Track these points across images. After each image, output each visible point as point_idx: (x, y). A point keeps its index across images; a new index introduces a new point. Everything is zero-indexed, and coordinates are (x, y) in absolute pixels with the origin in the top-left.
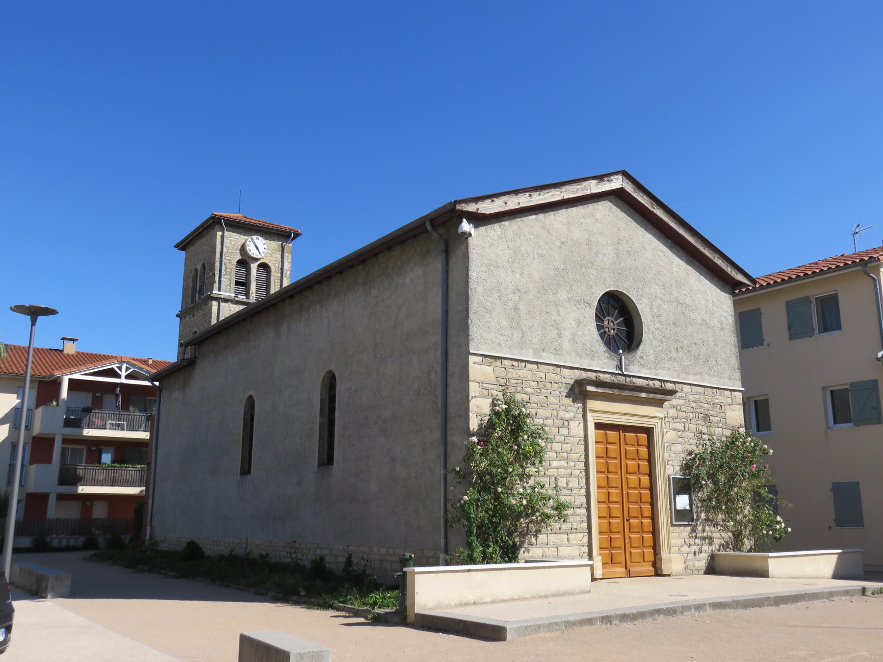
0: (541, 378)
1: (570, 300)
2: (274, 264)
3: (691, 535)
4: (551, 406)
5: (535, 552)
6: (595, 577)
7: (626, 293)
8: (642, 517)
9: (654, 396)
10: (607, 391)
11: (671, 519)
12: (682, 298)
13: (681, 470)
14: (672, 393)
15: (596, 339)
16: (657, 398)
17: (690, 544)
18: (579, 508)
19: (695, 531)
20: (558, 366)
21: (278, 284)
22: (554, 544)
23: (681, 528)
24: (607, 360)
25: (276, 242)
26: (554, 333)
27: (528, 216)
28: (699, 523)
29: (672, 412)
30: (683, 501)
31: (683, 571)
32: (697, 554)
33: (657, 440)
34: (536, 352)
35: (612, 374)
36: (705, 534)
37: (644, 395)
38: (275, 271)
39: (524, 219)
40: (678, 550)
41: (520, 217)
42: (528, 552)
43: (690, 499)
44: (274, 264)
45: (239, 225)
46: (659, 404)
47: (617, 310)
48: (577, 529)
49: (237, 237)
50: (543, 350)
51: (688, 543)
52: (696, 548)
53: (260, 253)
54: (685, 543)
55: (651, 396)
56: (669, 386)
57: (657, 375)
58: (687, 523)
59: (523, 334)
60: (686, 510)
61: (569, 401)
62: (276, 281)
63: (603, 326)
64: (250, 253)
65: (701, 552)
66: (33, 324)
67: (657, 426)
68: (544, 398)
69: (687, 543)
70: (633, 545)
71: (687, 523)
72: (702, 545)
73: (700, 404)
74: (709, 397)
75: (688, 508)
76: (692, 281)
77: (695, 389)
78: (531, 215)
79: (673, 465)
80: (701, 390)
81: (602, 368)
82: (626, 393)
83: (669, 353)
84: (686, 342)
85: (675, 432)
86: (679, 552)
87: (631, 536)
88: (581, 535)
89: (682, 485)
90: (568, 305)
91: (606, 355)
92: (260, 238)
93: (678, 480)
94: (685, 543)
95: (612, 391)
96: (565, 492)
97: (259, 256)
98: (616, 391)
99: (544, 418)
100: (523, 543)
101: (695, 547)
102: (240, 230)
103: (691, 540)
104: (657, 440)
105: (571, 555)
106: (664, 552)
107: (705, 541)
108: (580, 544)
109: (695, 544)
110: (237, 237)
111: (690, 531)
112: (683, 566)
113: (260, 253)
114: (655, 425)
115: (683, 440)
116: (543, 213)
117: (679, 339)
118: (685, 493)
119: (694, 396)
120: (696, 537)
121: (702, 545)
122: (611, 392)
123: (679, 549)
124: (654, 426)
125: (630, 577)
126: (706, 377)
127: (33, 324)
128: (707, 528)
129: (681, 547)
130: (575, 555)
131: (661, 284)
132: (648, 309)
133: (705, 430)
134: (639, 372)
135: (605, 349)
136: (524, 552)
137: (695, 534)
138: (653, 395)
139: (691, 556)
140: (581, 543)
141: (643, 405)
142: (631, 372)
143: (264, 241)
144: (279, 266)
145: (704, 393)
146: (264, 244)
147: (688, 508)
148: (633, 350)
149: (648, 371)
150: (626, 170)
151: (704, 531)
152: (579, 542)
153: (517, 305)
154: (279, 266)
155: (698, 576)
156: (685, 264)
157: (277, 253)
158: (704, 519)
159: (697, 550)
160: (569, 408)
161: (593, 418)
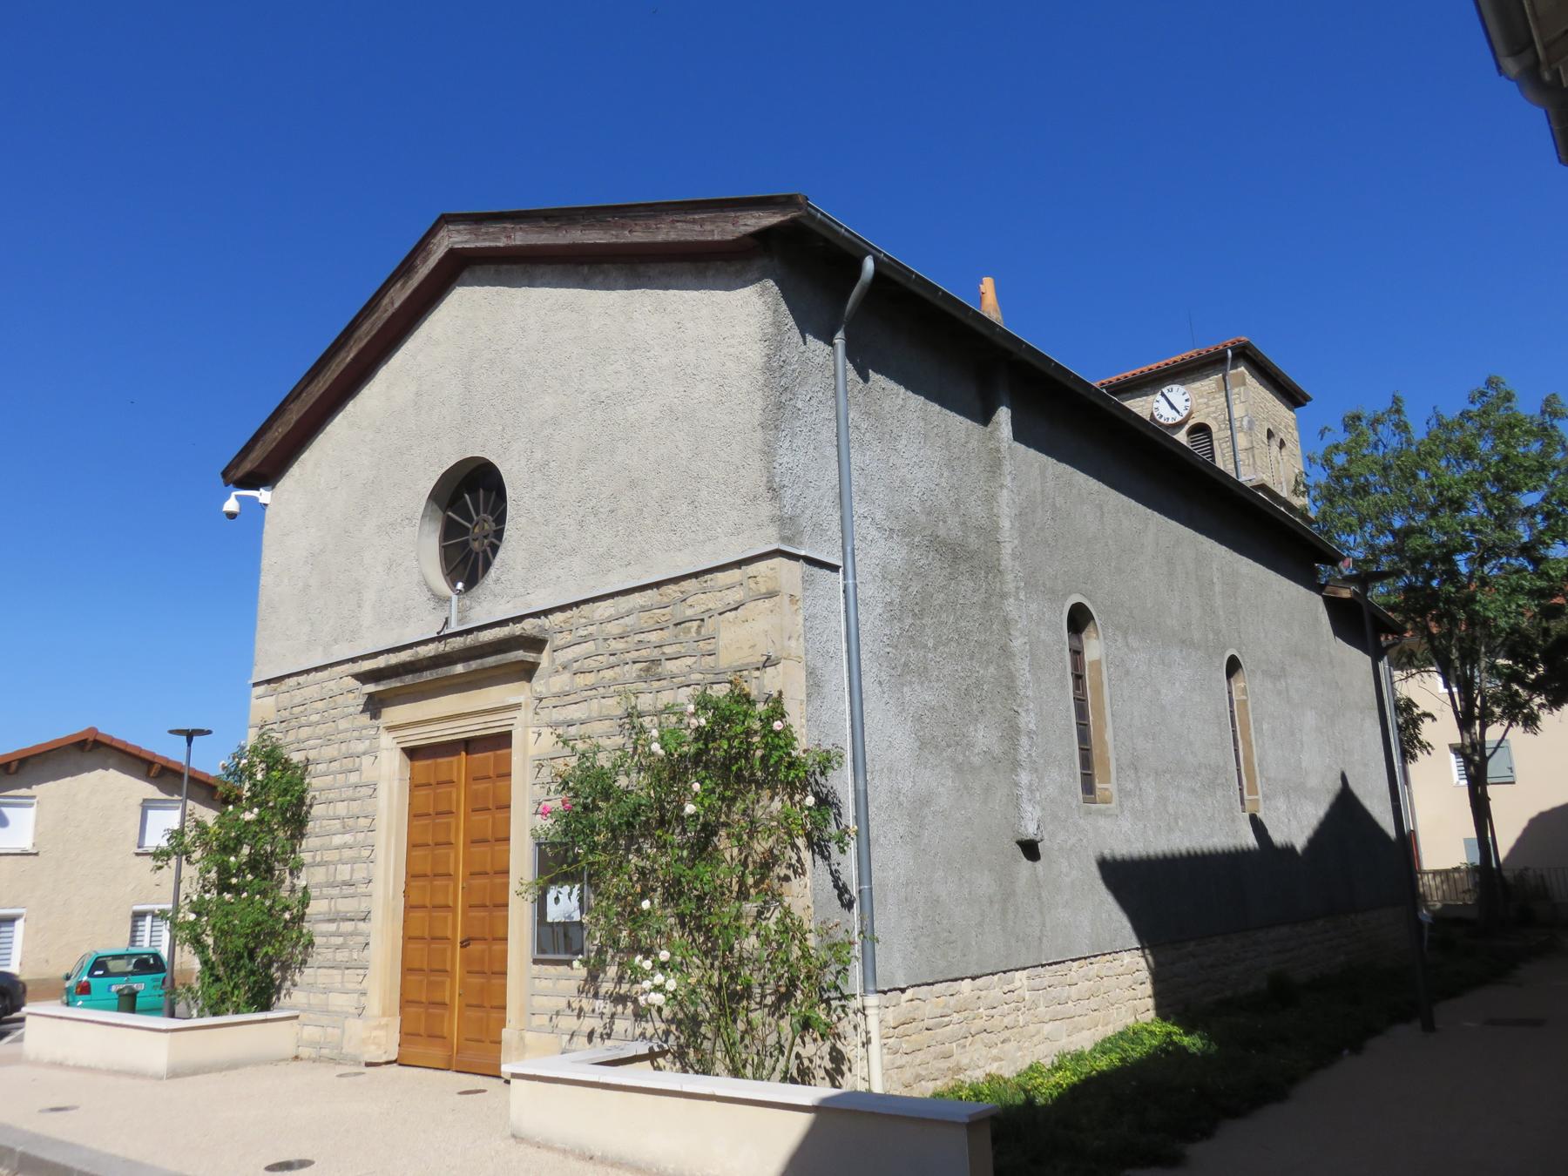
0: (332, 690)
2: (1215, 418)
5: (298, 997)
9: (482, 664)
10: (393, 685)
16: (487, 666)
17: (581, 1009)
21: (1229, 450)
25: (1211, 378)
29: (561, 682)
30: (564, 904)
32: (597, 1040)
37: (459, 668)
38: (1220, 430)
41: (321, 432)
42: (290, 997)
44: (1215, 418)
45: (1188, 366)
46: (527, 672)
49: (1141, 404)
51: (575, 1005)
52: (597, 1024)
53: (1178, 412)
54: (569, 1005)
55: (474, 665)
56: (529, 627)
62: (1224, 445)
64: (1162, 420)
65: (609, 1036)
66: (189, 745)
69: (574, 1006)
80: (735, 574)
82: (428, 676)
92: (1175, 387)
94: (569, 1005)
95: (401, 682)
97: (1179, 418)
98: (409, 679)
100: (284, 979)
101: (592, 1020)
102: (1146, 389)
107: (625, 1007)
109: (593, 1011)
110: (1141, 404)
113: (1178, 412)
121: (613, 1016)
122: (399, 685)
127: (189, 745)
130: (55, 1007)
136: (285, 996)
138: (479, 661)
141: (480, 688)
143: (1182, 389)
144: (1225, 417)
146: (1184, 394)
148: (483, 576)
150: (444, 212)
154: (1225, 417)
157: (1216, 396)
159: (599, 1030)
161: (396, 741)
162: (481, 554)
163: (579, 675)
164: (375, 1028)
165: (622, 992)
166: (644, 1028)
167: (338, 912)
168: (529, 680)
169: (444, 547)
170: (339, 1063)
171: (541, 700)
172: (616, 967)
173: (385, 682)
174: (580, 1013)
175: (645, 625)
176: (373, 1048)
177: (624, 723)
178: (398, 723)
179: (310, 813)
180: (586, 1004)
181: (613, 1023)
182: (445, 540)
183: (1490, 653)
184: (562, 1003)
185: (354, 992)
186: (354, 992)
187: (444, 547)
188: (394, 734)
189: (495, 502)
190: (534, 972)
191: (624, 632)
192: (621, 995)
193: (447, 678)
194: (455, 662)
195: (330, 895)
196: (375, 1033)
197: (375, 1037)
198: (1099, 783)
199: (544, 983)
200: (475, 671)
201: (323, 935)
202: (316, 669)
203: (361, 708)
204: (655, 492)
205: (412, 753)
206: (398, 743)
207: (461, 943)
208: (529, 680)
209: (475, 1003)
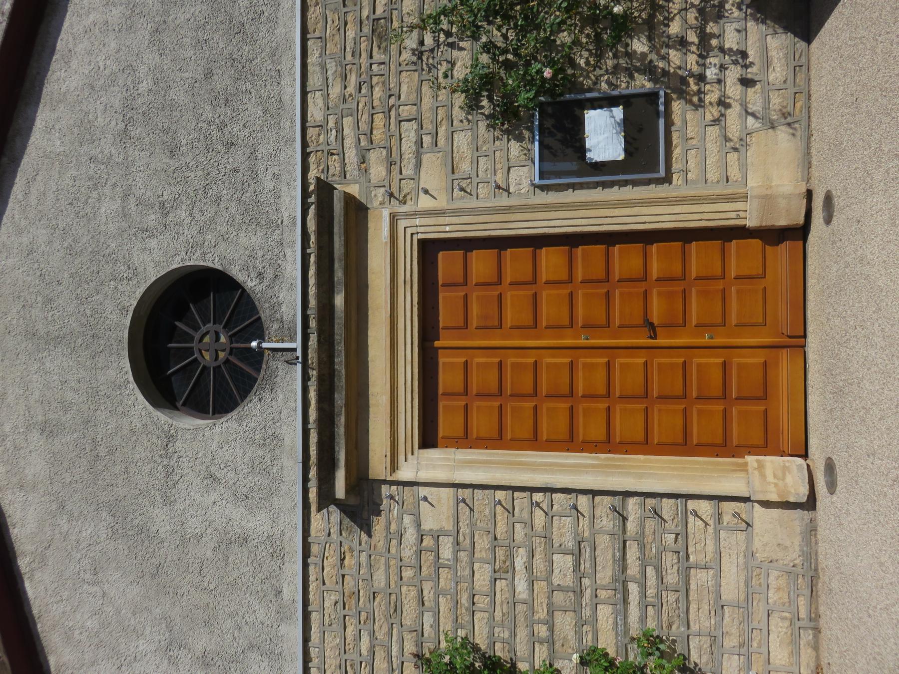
0: (336, 603)
1: (168, 501)
3: (695, 99)
4: (393, 585)
6: (804, 499)
7: (130, 314)
8: (645, 278)
9: (340, 260)
11: (648, 182)
12: (113, 123)
13: (520, 138)
14: (325, 189)
15: (236, 426)
18: (625, 519)
19: (684, 81)
20: (306, 554)
22: (713, 613)
23: (675, 136)
24: (279, 392)
26: (238, 554)
27: (27, 599)
28: (661, 64)
31: (798, 134)
33: (448, 228)
34: (283, 616)
35: (306, 378)
36: (692, 37)
37: (339, 300)
39: (35, 611)
40: (736, 154)
41: (35, 625)
43: (596, 104)
47: (177, 323)
48: (677, 535)
50: (279, 593)
55: (339, 274)
57: (294, 220)
58: (662, 122)
59: (251, 647)
60: (626, 120)
61: (379, 525)
63: (214, 368)
65: (744, 54)
67: (414, 230)
68: (377, 600)
70: (719, 272)
71: (662, 122)
72: (722, 49)
73: (349, 57)
74: (329, 22)
75: (618, 112)
76: (74, 84)
77: (315, 80)
78: (25, 593)
79: (509, 169)
81: (295, 410)
83: (239, 175)
84: (208, 113)
85: (426, 158)
86: (743, 150)
87: (694, 323)
88: (694, 524)
89: (559, 136)
90: (179, 506)
91: (267, 396)
93: (546, 152)
96: (588, 565)
98: (340, 399)
99: (476, 154)
101: (729, 82)
103: (708, 98)
104: (448, 228)
105: (741, 560)
106: (742, 214)
108: (715, 529)
109: (719, 81)
111: (682, 102)
112: (782, 134)
114: (412, 234)
115: (444, 128)
116: (15, 558)
117: (205, 137)
118: (579, 124)
119: (330, 80)
120: (701, 78)
123: (735, 149)
124: (415, 238)
125: (805, 336)
126: (280, 30)
128: (675, 28)
129: (727, 139)
131: (94, 194)
132: (153, 243)
133: (411, 42)
134: (292, 287)
135: (255, 399)
137: (691, 81)
138: (336, 265)
139: (754, 96)
140: (711, 522)
141: (367, 286)
142: (295, 316)
145: (320, 38)
147: (618, 112)
149: (289, 252)
151: (682, 43)
152: (710, 529)
153: (198, 657)
155: (812, 67)
156: (41, 106)
158: (650, 39)
160: (393, 527)
162: (232, 358)
163: (373, 137)
164: (763, 476)
165: (696, 40)
166: (733, 5)
167: (614, 580)
168: (367, 209)
169: (214, 414)
170: (816, 570)
171: (391, 195)
172: (671, 51)
173: (337, 449)
174: (723, 103)
175: (339, 46)
176: (789, 479)
177: (427, 64)
178: (389, 449)
179: (484, 653)
180: (712, 97)
181: (730, 50)
182: (207, 412)
183: (528, 84)
184: (713, 132)
185: (717, 538)
186: (717, 538)
187: (214, 414)
188: (401, 457)
189: (187, 325)
190: (680, 182)
191: (341, 75)
192: (700, 42)
193: (347, 325)
194: (332, 306)
195: (591, 600)
196: (770, 478)
197: (775, 476)
198: (583, 250)
199: (692, 164)
200: (346, 274)
201: (643, 619)
202: (306, 639)
203: (364, 537)
204: (222, 45)
205: (428, 440)
206: (412, 454)
207: (651, 338)
208: (367, 209)
209: (720, 303)
